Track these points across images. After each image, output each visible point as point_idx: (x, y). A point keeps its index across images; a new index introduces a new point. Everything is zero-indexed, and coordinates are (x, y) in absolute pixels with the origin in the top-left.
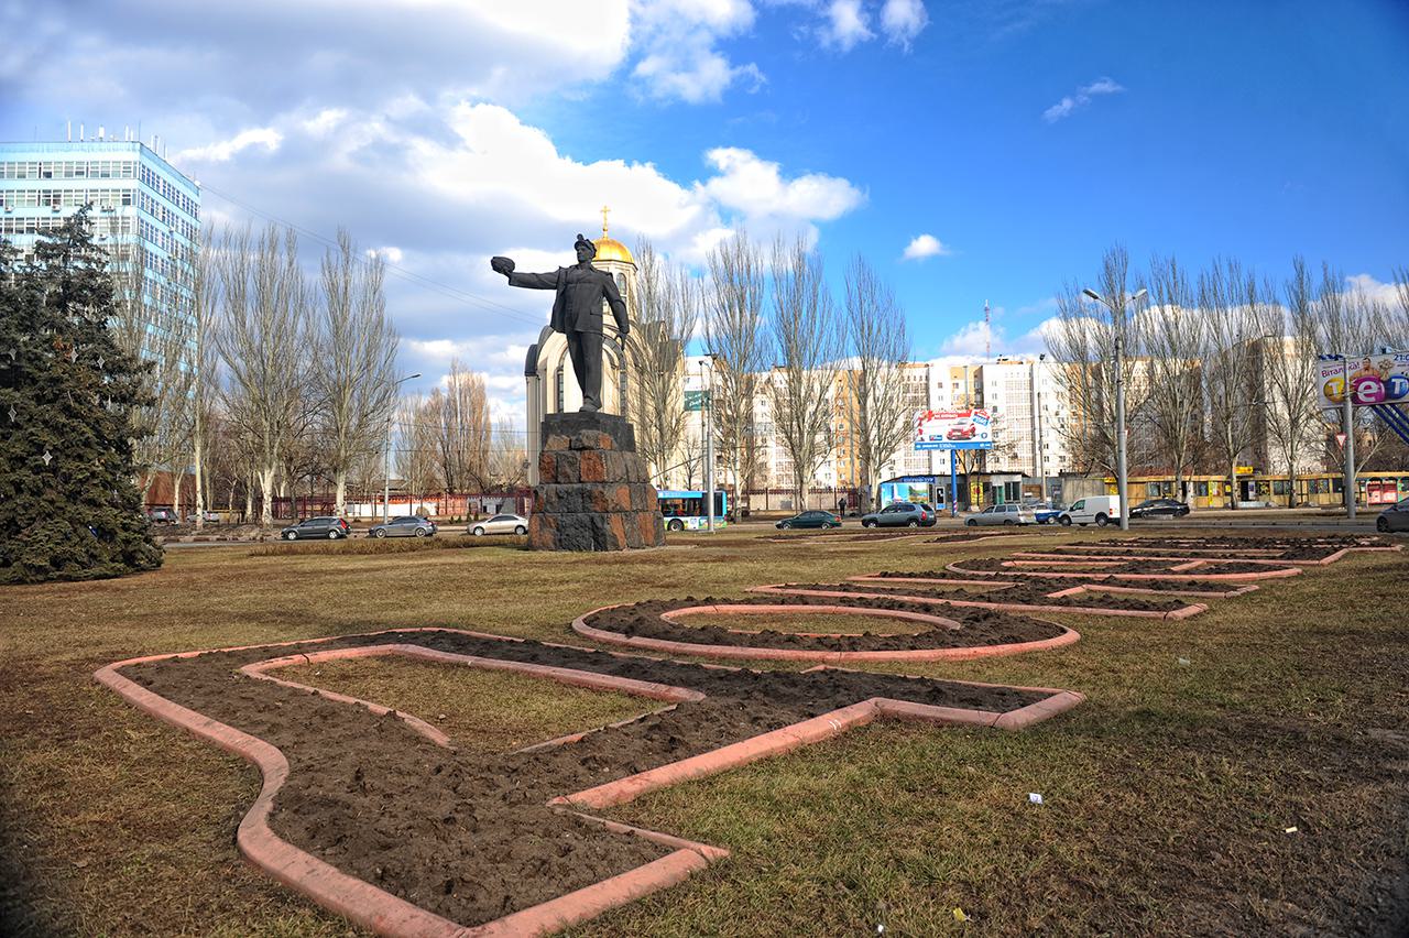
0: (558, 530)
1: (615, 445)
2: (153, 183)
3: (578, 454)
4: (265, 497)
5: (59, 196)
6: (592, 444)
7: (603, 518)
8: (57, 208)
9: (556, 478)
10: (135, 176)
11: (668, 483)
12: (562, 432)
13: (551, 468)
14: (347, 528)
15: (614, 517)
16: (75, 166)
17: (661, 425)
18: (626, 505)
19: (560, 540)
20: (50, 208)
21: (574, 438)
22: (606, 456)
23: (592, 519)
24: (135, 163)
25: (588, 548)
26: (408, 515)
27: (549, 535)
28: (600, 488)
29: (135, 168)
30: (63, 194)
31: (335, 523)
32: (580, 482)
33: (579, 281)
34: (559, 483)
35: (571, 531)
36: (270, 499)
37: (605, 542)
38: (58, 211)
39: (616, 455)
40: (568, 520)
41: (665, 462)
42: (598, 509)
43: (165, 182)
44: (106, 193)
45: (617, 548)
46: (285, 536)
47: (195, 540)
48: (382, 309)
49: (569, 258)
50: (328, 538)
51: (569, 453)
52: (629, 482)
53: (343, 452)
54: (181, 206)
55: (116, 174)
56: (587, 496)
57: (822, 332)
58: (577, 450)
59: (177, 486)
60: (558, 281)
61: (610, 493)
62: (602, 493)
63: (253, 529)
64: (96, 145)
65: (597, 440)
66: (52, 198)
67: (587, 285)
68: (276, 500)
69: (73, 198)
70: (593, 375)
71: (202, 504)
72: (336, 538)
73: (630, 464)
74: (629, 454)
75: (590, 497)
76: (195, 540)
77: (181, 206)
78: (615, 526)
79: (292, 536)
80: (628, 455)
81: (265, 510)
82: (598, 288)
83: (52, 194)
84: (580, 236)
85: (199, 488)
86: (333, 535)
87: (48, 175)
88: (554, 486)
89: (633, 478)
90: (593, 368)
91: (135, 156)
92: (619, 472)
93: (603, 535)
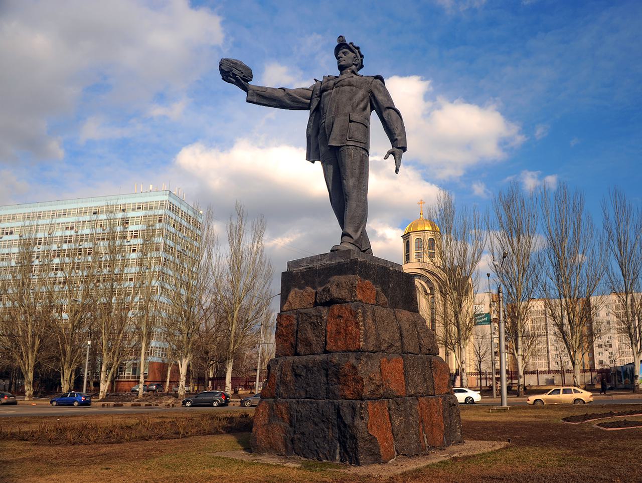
0: (291, 426)
1: (383, 298)
3: (324, 311)
4: (181, 377)
5: (128, 220)
6: (344, 294)
7: (354, 409)
9: (294, 347)
11: (464, 366)
12: (307, 284)
15: (370, 406)
16: (137, 205)
17: (458, 322)
18: (395, 385)
19: (292, 440)
21: (320, 289)
22: (364, 313)
23: (338, 410)
24: (166, 201)
28: (353, 361)
30: (130, 219)
31: (218, 395)
32: (326, 352)
36: (185, 379)
37: (355, 449)
39: (382, 312)
41: (461, 350)
42: (347, 393)
45: (378, 459)
49: (328, 67)
50: (213, 406)
51: (312, 311)
52: (403, 353)
53: (232, 346)
56: (332, 372)
59: (169, 371)
61: (368, 370)
62: (354, 368)
63: (170, 398)
65: (352, 289)
69: (135, 221)
72: (217, 406)
73: (406, 326)
74: (406, 312)
75: (336, 375)
78: (373, 422)
79: (188, 404)
80: (404, 315)
81: (180, 386)
86: (215, 404)
88: (290, 359)
89: (411, 346)
90: (354, 195)
91: (166, 198)
92: (386, 336)
93: (353, 437)
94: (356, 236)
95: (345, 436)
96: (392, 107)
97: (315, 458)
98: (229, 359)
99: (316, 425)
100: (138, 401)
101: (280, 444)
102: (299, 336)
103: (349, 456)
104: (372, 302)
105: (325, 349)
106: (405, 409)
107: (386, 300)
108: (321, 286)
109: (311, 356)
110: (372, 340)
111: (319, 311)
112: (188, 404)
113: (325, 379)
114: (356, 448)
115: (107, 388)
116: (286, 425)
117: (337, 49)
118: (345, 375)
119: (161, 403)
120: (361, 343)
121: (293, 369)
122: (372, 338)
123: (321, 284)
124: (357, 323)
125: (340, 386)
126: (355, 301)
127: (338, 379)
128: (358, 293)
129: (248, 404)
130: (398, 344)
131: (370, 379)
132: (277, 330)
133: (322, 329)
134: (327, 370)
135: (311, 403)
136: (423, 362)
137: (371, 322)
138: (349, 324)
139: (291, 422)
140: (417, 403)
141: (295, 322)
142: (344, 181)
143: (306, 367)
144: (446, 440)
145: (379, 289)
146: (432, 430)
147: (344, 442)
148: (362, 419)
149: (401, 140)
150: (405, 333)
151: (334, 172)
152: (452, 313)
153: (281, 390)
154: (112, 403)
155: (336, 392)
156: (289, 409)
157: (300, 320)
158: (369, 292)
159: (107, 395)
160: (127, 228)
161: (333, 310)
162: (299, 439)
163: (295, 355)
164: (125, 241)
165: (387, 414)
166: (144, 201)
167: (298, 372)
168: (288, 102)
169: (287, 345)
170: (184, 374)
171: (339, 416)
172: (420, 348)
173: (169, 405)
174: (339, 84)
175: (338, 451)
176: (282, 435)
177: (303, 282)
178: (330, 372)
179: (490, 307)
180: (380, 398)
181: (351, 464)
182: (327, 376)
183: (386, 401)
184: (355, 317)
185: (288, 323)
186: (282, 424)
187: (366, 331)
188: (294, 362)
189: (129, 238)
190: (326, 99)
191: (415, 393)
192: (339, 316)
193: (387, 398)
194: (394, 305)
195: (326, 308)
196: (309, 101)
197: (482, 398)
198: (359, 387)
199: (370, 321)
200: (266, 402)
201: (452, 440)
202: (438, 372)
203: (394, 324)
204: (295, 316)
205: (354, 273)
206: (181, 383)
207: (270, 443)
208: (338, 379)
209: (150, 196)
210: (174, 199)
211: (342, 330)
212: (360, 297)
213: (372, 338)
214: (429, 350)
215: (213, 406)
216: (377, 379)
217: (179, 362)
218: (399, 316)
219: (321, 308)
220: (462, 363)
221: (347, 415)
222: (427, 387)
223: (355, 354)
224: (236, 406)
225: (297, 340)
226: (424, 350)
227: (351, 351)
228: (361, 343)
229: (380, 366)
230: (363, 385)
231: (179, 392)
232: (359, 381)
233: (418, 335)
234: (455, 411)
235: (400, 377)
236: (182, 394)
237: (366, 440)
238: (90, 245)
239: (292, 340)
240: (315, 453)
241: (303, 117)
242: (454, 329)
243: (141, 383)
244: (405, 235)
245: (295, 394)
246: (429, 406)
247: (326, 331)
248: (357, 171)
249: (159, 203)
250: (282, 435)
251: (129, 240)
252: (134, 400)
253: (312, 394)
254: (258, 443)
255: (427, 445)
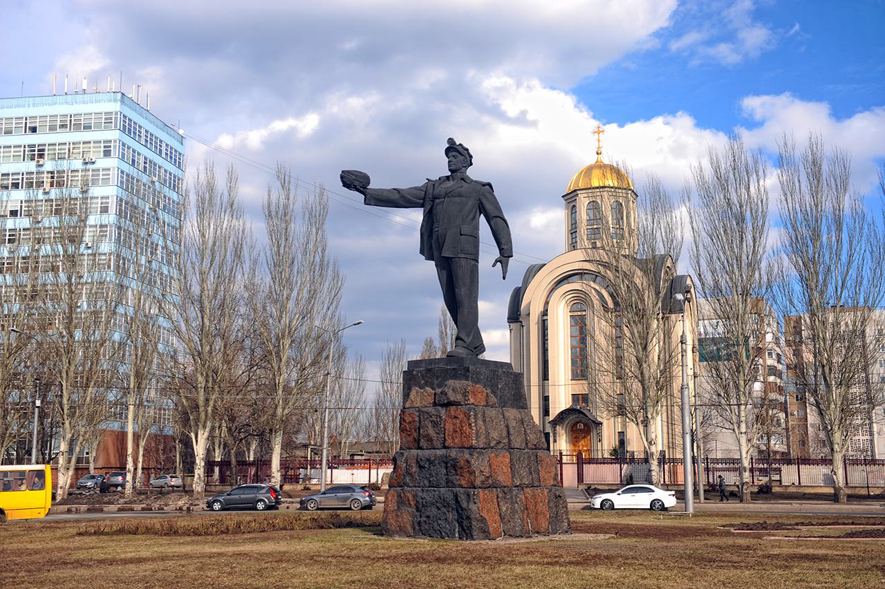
0: (417, 511)
1: (493, 399)
2: (135, 133)
3: (443, 411)
4: (198, 461)
5: (43, 150)
6: (459, 398)
8: (41, 163)
9: (417, 441)
10: (116, 126)
12: (426, 384)
13: (413, 429)
14: (276, 498)
15: (481, 494)
18: (503, 477)
19: (419, 523)
20: (33, 164)
23: (456, 496)
24: (116, 113)
25: (451, 535)
26: (576, 465)
27: (407, 518)
28: (467, 456)
29: (116, 118)
30: (47, 148)
31: (264, 491)
32: (445, 447)
33: (446, 195)
34: (421, 449)
35: (433, 511)
36: (203, 464)
38: (42, 166)
39: (491, 413)
40: (428, 497)
42: (463, 482)
43: (147, 131)
44: (88, 145)
45: (487, 535)
46: (210, 505)
47: (120, 510)
48: (323, 250)
51: (432, 410)
52: (510, 448)
53: (279, 410)
54: (164, 155)
55: (98, 126)
56: (452, 466)
57: (851, 256)
58: (443, 405)
60: (426, 198)
61: (480, 464)
62: (468, 462)
64: (79, 97)
65: (465, 394)
66: (36, 153)
67: (457, 199)
68: (210, 465)
70: (466, 311)
71: (132, 469)
73: (513, 424)
76: (120, 510)
77: (164, 155)
78: (484, 506)
79: (217, 506)
80: (512, 413)
81: (196, 476)
82: (471, 203)
83: (36, 149)
84: (451, 141)
85: (130, 451)
86: (260, 506)
87: (34, 130)
88: (414, 452)
89: (517, 442)
91: (115, 107)
92: (495, 435)
93: (468, 518)
94: (468, 340)
95: (462, 518)
96: (500, 216)
97: (439, 537)
98: (276, 432)
99: (439, 509)
100: (126, 503)
101: (409, 528)
102: (421, 432)
103: (466, 533)
104: (482, 404)
105: (444, 445)
106: (511, 498)
107: (496, 400)
108: (439, 388)
109: (433, 450)
110: (483, 439)
111: (438, 411)
112: (217, 506)
113: (445, 471)
114: (471, 526)
115: (69, 481)
116: (413, 510)
117: (448, 151)
118: (462, 468)
119: (166, 505)
120: (474, 442)
121: (417, 461)
122: (483, 437)
123: (440, 386)
124: (470, 424)
125: (458, 477)
126: (469, 404)
127: (456, 470)
128: (470, 397)
129: (312, 506)
130: (506, 441)
131: (481, 471)
132: (400, 425)
133: (441, 428)
134: (446, 463)
135: (434, 491)
136: (529, 457)
137: (481, 423)
138: (463, 425)
139: (417, 508)
140: (522, 492)
141: (417, 419)
142: (457, 290)
143: (428, 460)
144: (552, 528)
145: (489, 391)
146: (537, 517)
147: (461, 522)
148: (475, 503)
149: (507, 249)
150: (512, 431)
151: (447, 276)
152: (634, 359)
153: (408, 479)
154: (84, 507)
155: (454, 482)
156: (415, 496)
157: (421, 417)
158: (479, 395)
159: (70, 494)
160: (42, 166)
161: (450, 411)
162: (425, 521)
163: (418, 449)
164: (41, 191)
165: (495, 501)
166: (73, 112)
167: (422, 464)
168: (402, 202)
169: (410, 439)
170: (202, 456)
171: (457, 502)
172: (527, 444)
173: (181, 509)
174: (449, 195)
175: (457, 530)
176: (410, 519)
177: (423, 382)
178: (449, 465)
179: (693, 352)
180: (489, 487)
181: (467, 539)
182: (446, 468)
183: (494, 489)
184: (469, 419)
185: (411, 419)
186: (410, 509)
187: (477, 431)
188: (418, 455)
189: (47, 186)
190: (438, 207)
191: (520, 484)
192: (456, 417)
193: (496, 488)
194: (503, 404)
195: (444, 409)
196: (422, 201)
197: (677, 503)
198: (472, 478)
199: (480, 422)
200: (394, 490)
201: (558, 529)
202: (544, 465)
203: (502, 423)
204: (417, 414)
205: (467, 379)
206: (197, 472)
207: (400, 526)
208: (456, 470)
209: (84, 102)
210: (130, 108)
211: (458, 430)
212: (472, 400)
213: (483, 437)
214: (535, 445)
215: (255, 509)
216: (487, 471)
217: (193, 435)
218: (507, 414)
219: (440, 408)
220: (650, 443)
221: (463, 501)
222: (532, 479)
223: (469, 450)
224: (291, 509)
225: (419, 436)
226: (530, 445)
227: (465, 448)
228: (474, 442)
229: (489, 461)
230: (475, 477)
231: (194, 486)
232: (472, 473)
233: (525, 431)
234: (561, 502)
235: (507, 470)
236: (200, 490)
237: (478, 521)
238: (24, 222)
239: (415, 435)
240: (438, 532)
241: (416, 216)
242: (636, 386)
243: (129, 471)
244: (568, 194)
245: (419, 483)
246: (534, 496)
247: (445, 429)
248: (468, 281)
249: (104, 117)
250: (410, 519)
251: (47, 190)
252: (118, 500)
253: (435, 483)
254: (389, 527)
255: (531, 529)
